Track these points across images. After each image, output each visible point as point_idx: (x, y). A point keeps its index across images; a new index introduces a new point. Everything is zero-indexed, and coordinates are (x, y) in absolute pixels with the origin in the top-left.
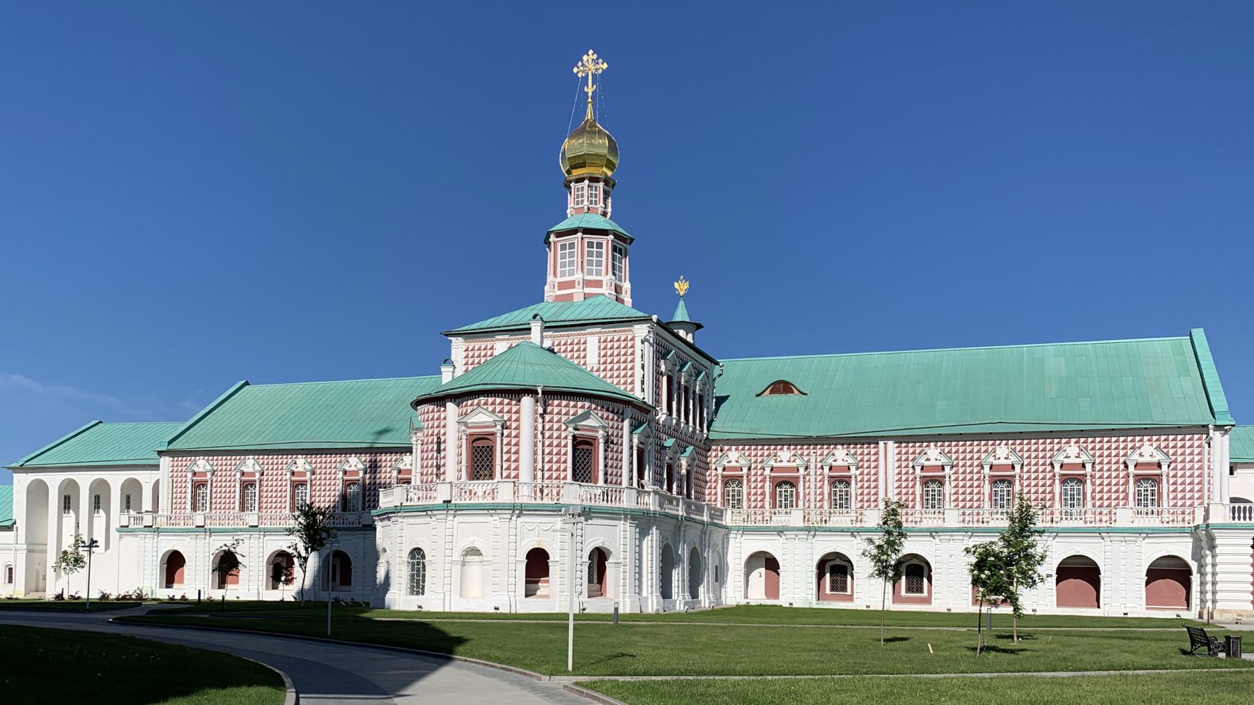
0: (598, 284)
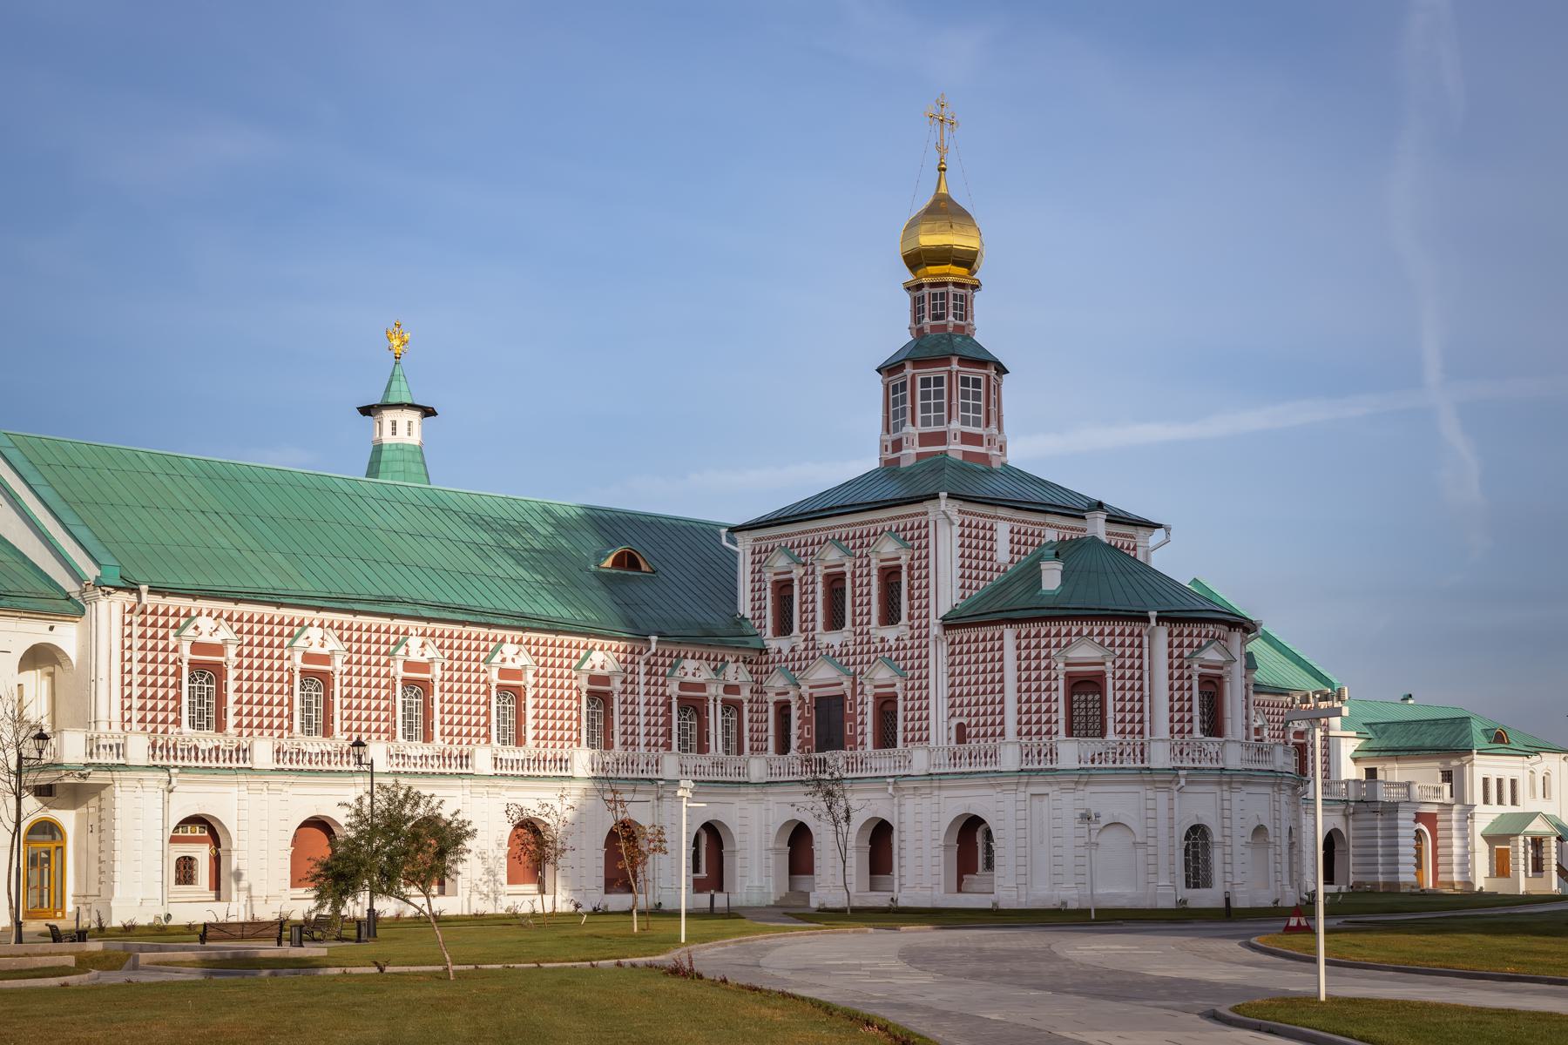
0: (941, 438)
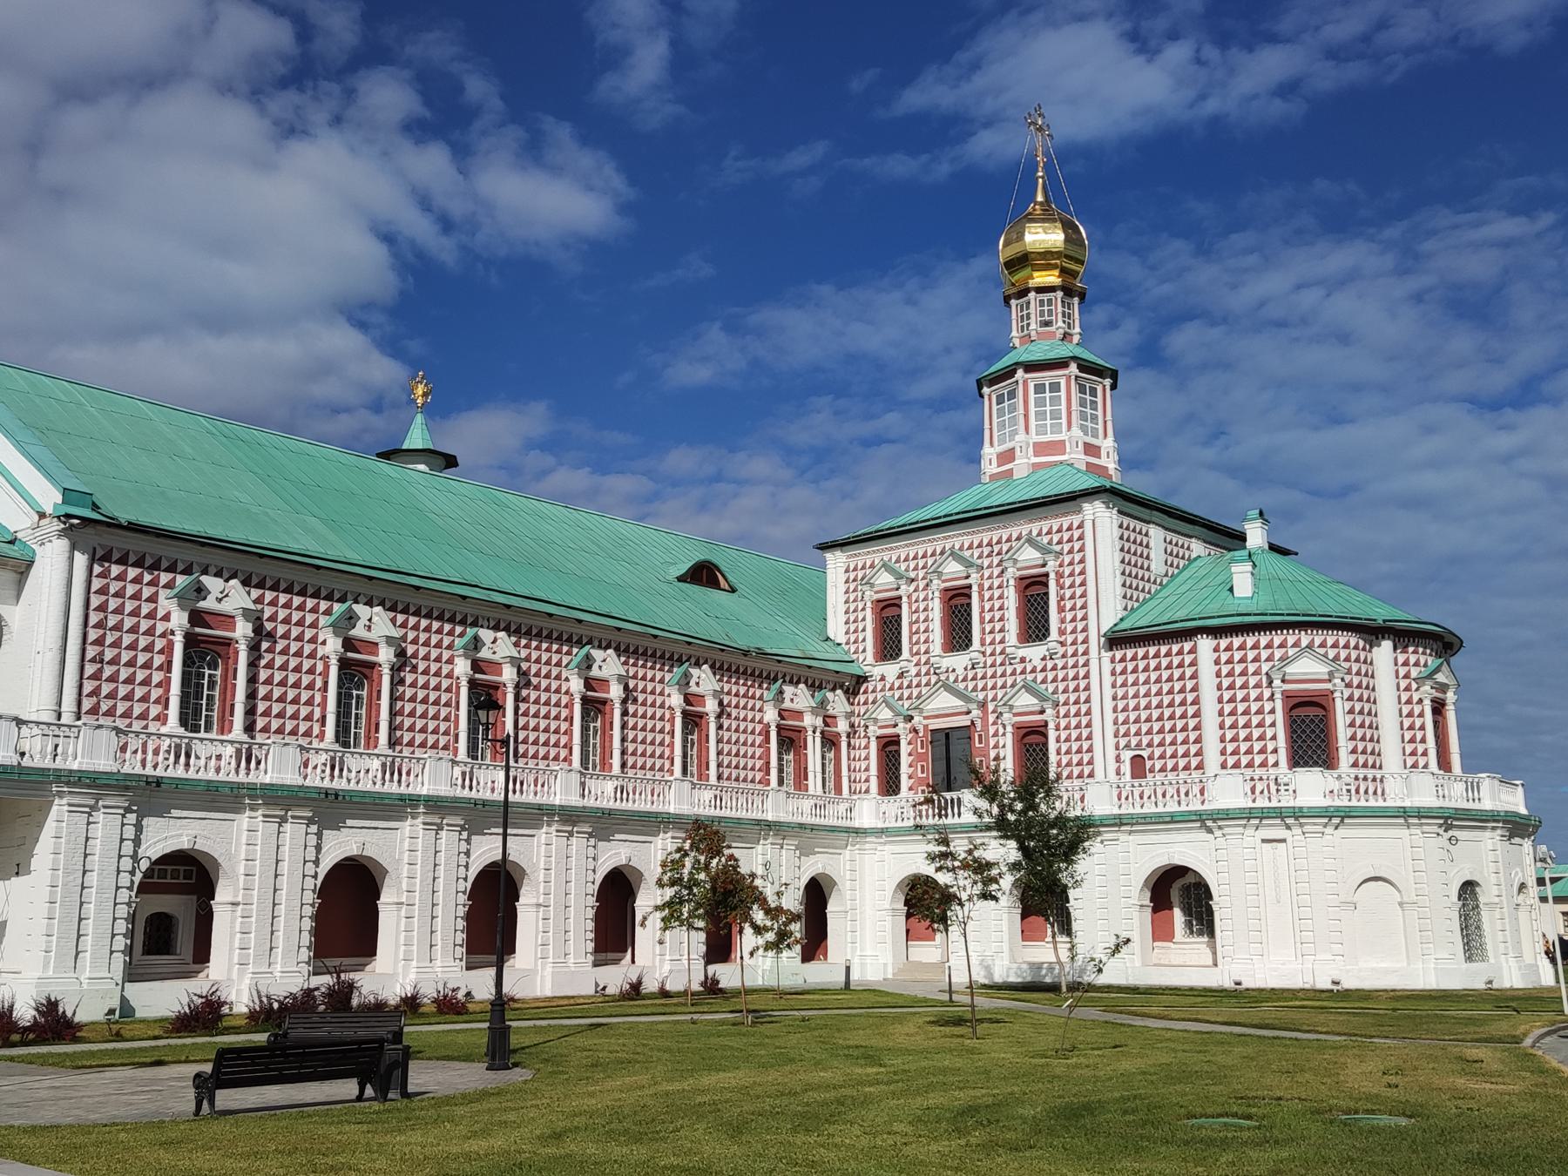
0: (1059, 447)
